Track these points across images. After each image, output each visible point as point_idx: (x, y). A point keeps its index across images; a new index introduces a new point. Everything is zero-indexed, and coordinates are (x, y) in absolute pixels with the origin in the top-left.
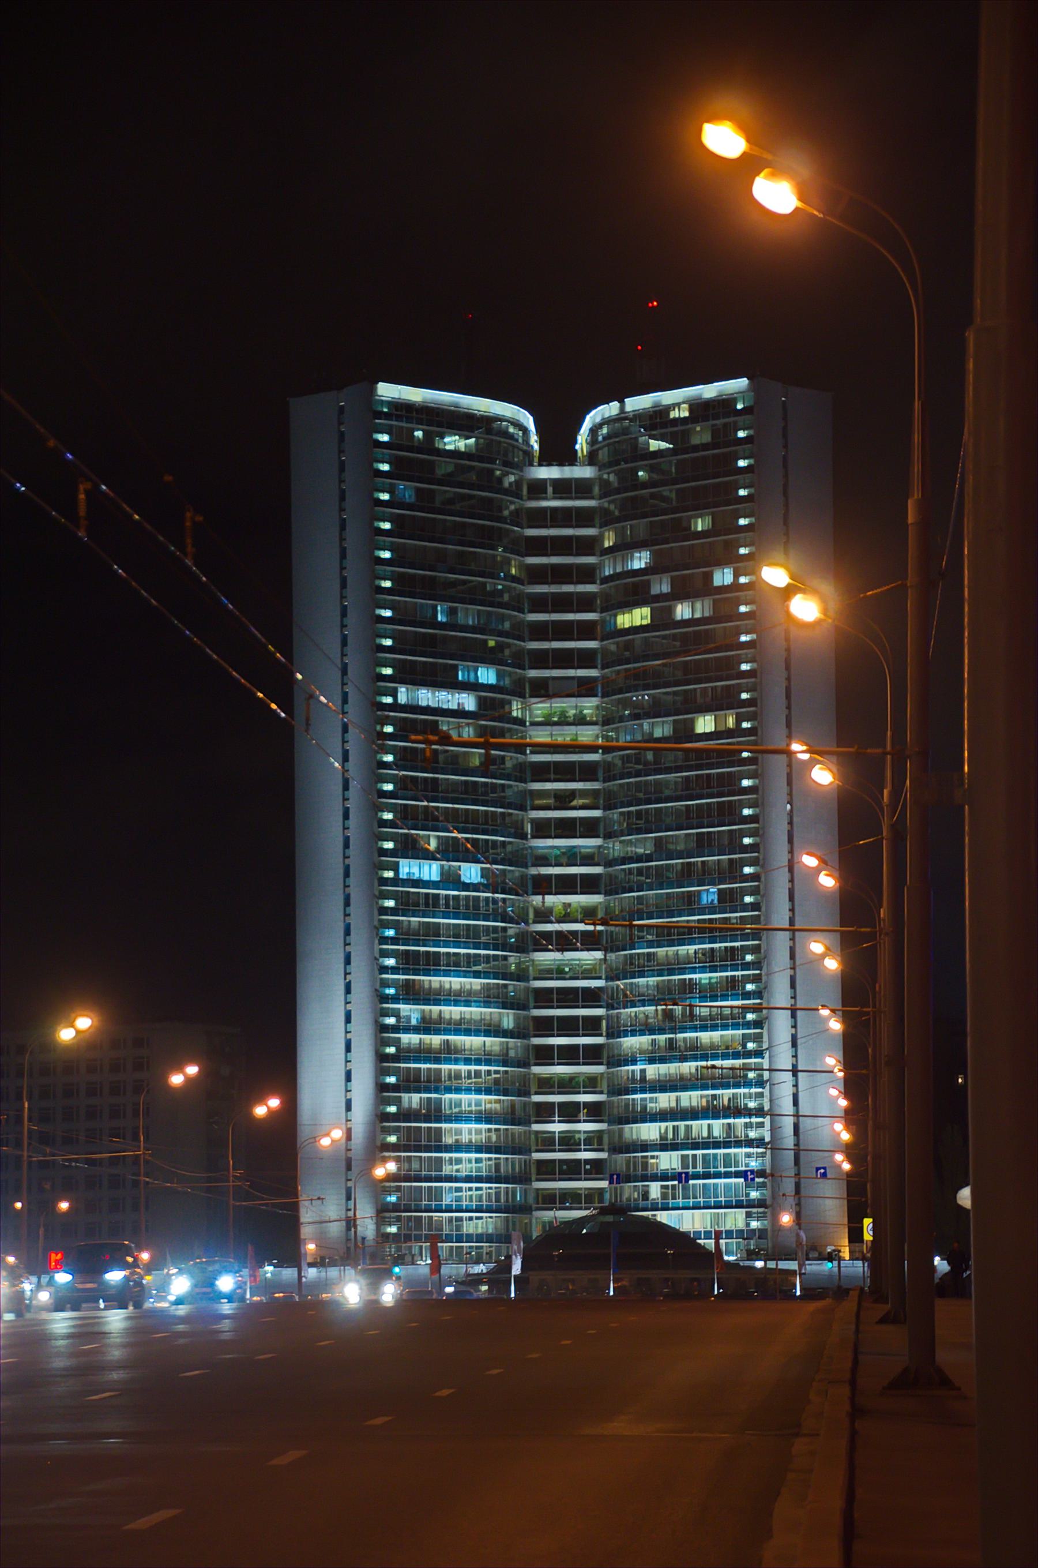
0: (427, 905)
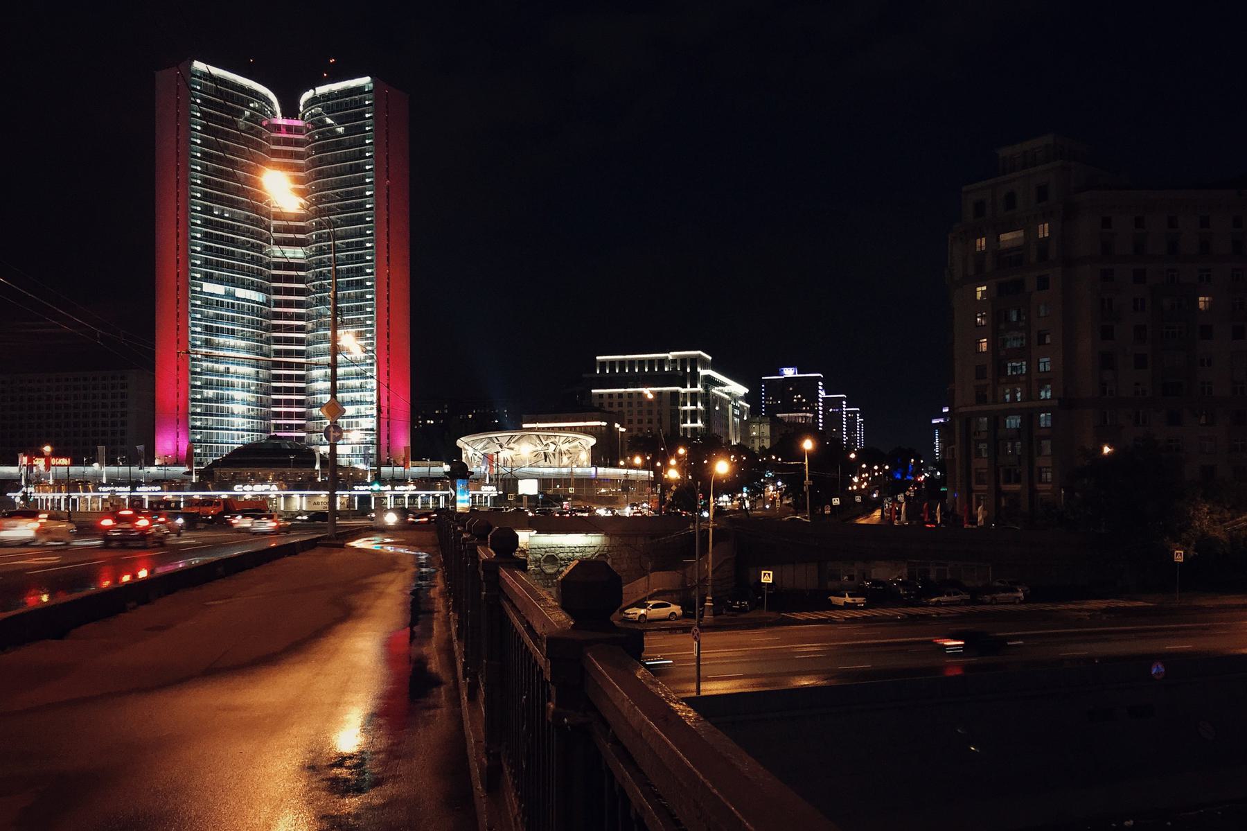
0: (217, 305)
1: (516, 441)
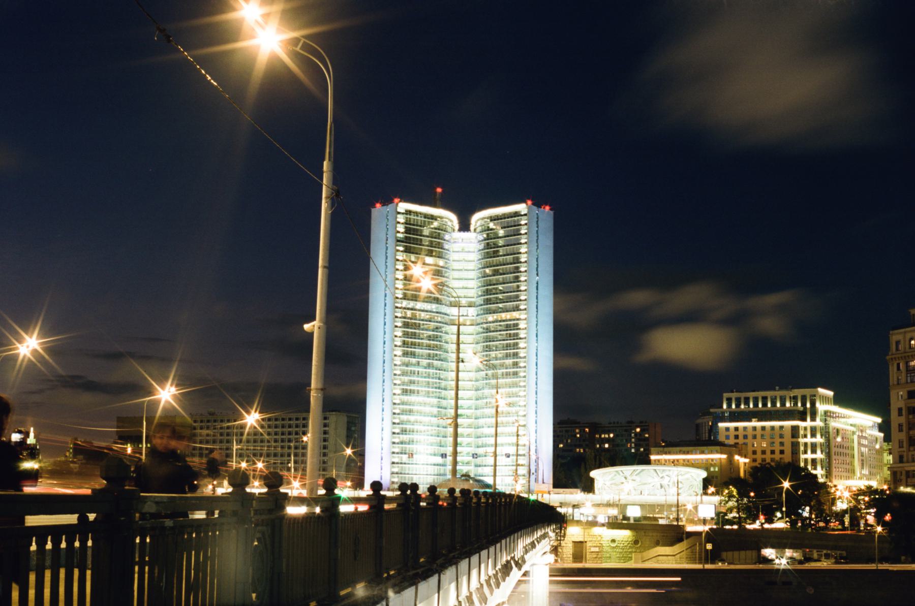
1: (638, 474)
